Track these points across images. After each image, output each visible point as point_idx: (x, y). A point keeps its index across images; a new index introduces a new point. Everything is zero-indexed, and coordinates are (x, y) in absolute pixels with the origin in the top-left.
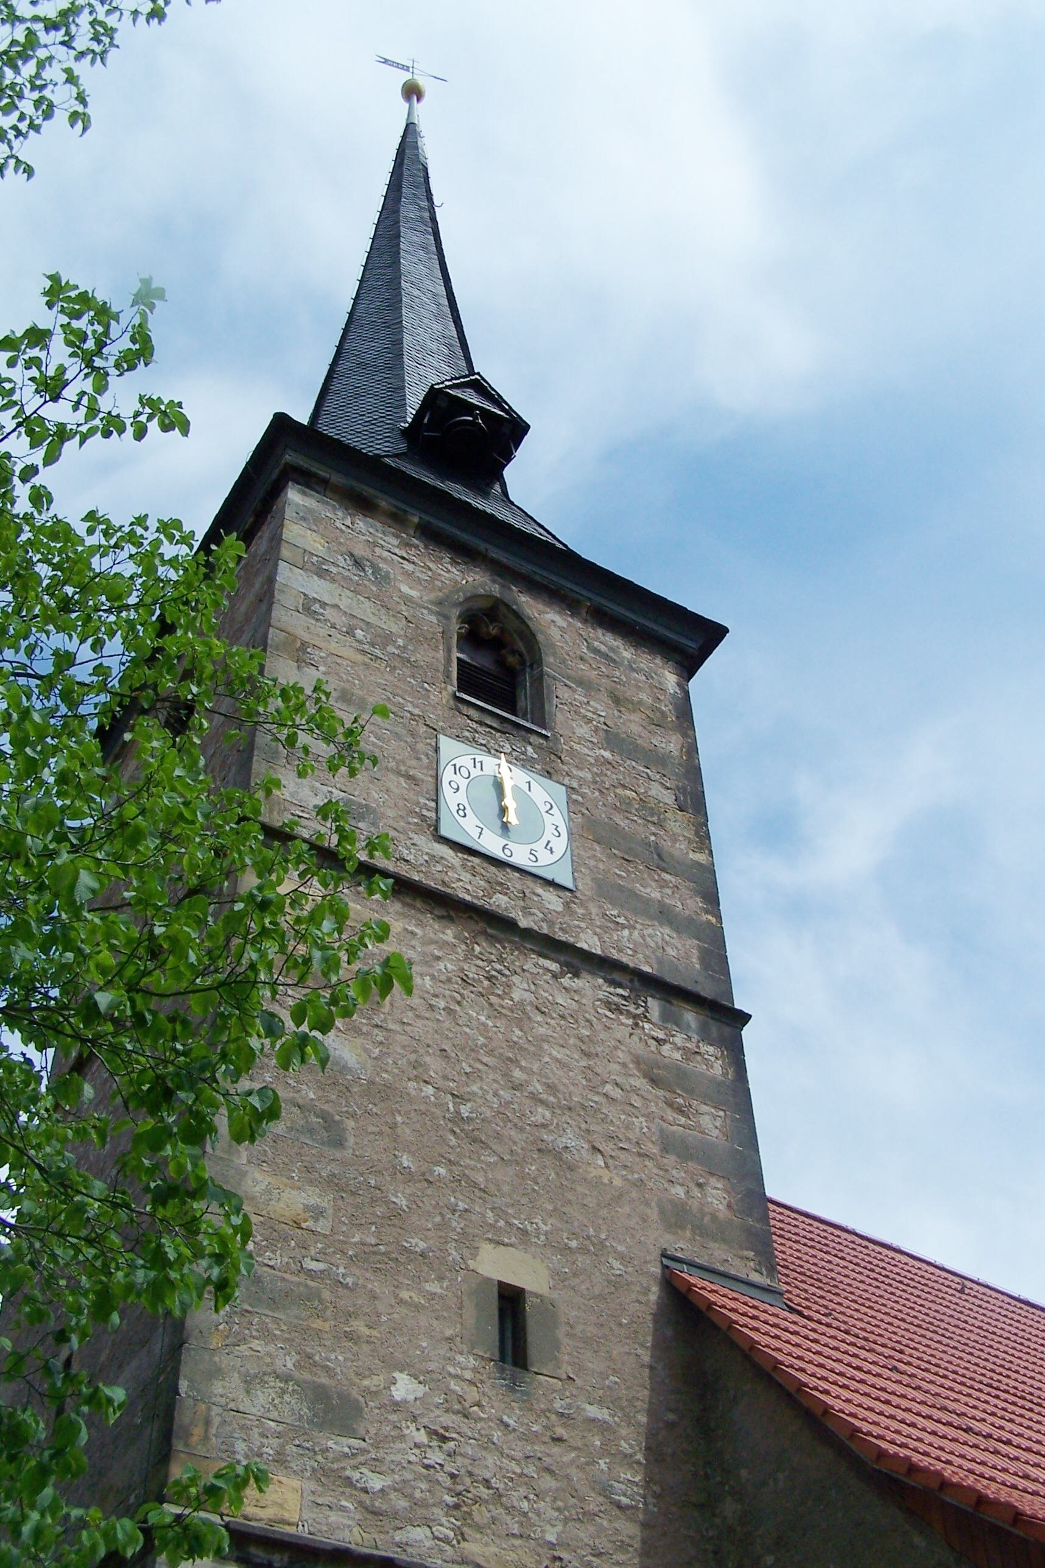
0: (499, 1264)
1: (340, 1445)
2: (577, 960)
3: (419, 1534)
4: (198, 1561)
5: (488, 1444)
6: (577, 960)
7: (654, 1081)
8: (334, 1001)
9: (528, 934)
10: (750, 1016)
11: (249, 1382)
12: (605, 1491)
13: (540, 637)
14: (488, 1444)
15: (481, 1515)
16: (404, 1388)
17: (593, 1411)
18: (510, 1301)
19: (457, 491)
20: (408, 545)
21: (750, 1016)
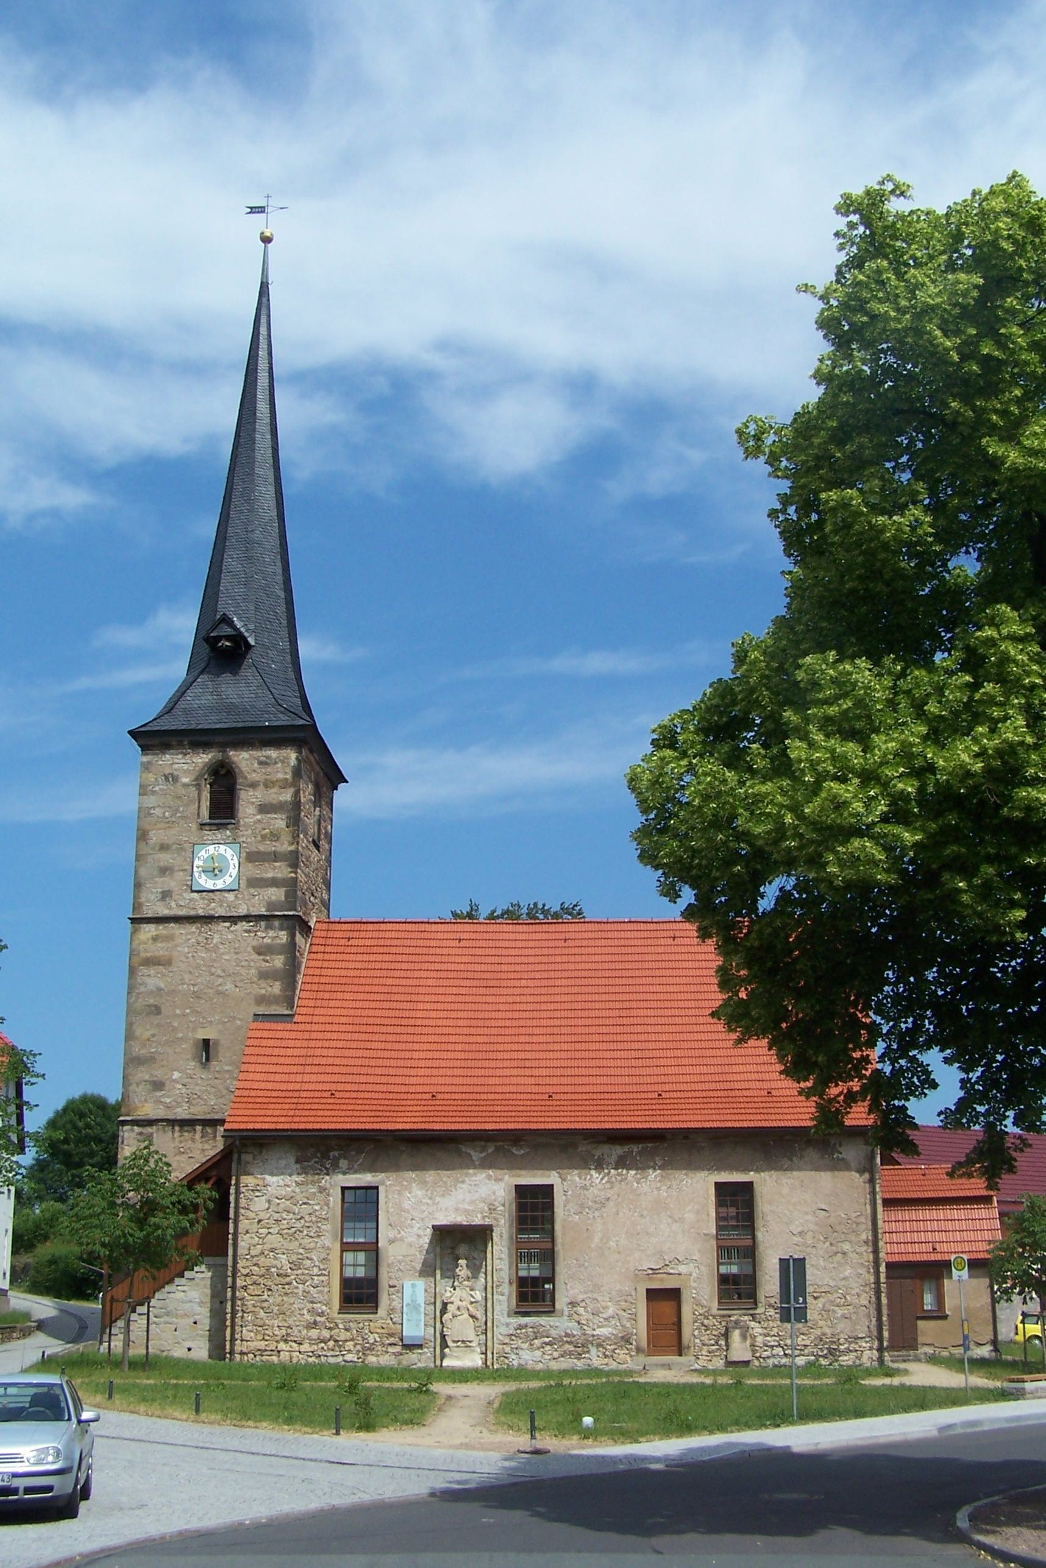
0: (202, 1035)
1: (158, 1094)
2: (234, 920)
3: (179, 1110)
4: (821, 334)
5: (197, 1085)
6: (234, 920)
7: (259, 954)
8: (996, 721)
9: (220, 917)
10: (716, 1183)
11: (138, 1085)
12: (227, 1089)
13: (237, 770)
14: (197, 1085)
15: (194, 1102)
16: (176, 1075)
17: (227, 1068)
18: (206, 1042)
19: (512, 1386)
20: (185, 754)
21: (716, 1183)
